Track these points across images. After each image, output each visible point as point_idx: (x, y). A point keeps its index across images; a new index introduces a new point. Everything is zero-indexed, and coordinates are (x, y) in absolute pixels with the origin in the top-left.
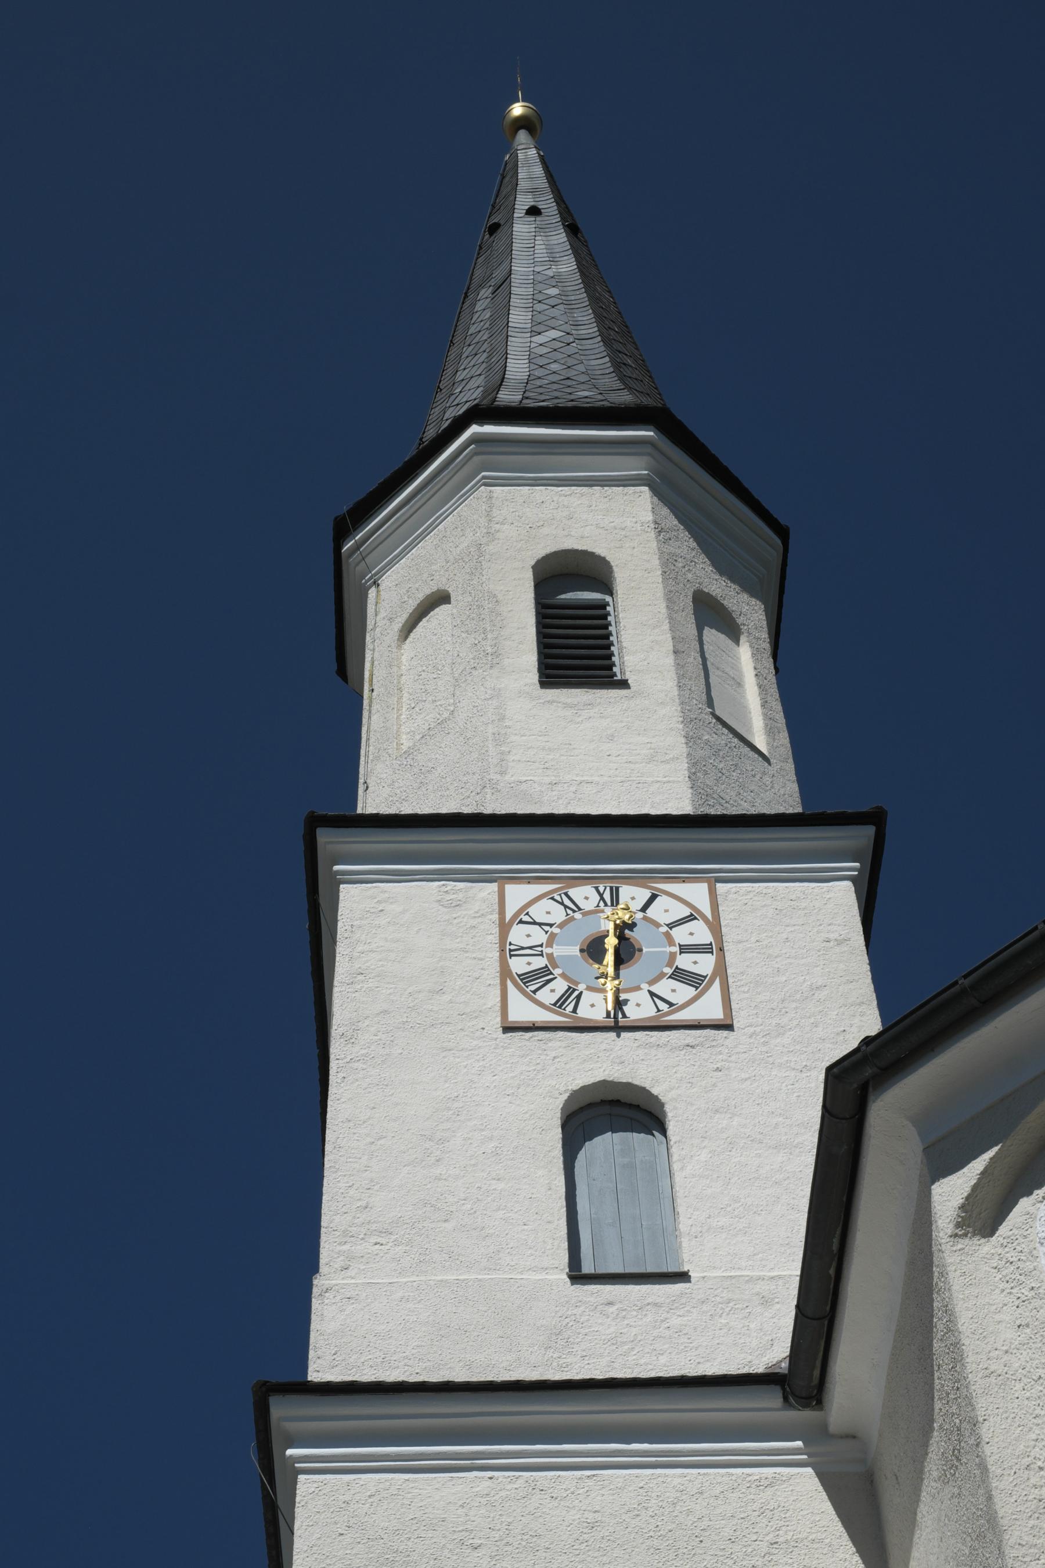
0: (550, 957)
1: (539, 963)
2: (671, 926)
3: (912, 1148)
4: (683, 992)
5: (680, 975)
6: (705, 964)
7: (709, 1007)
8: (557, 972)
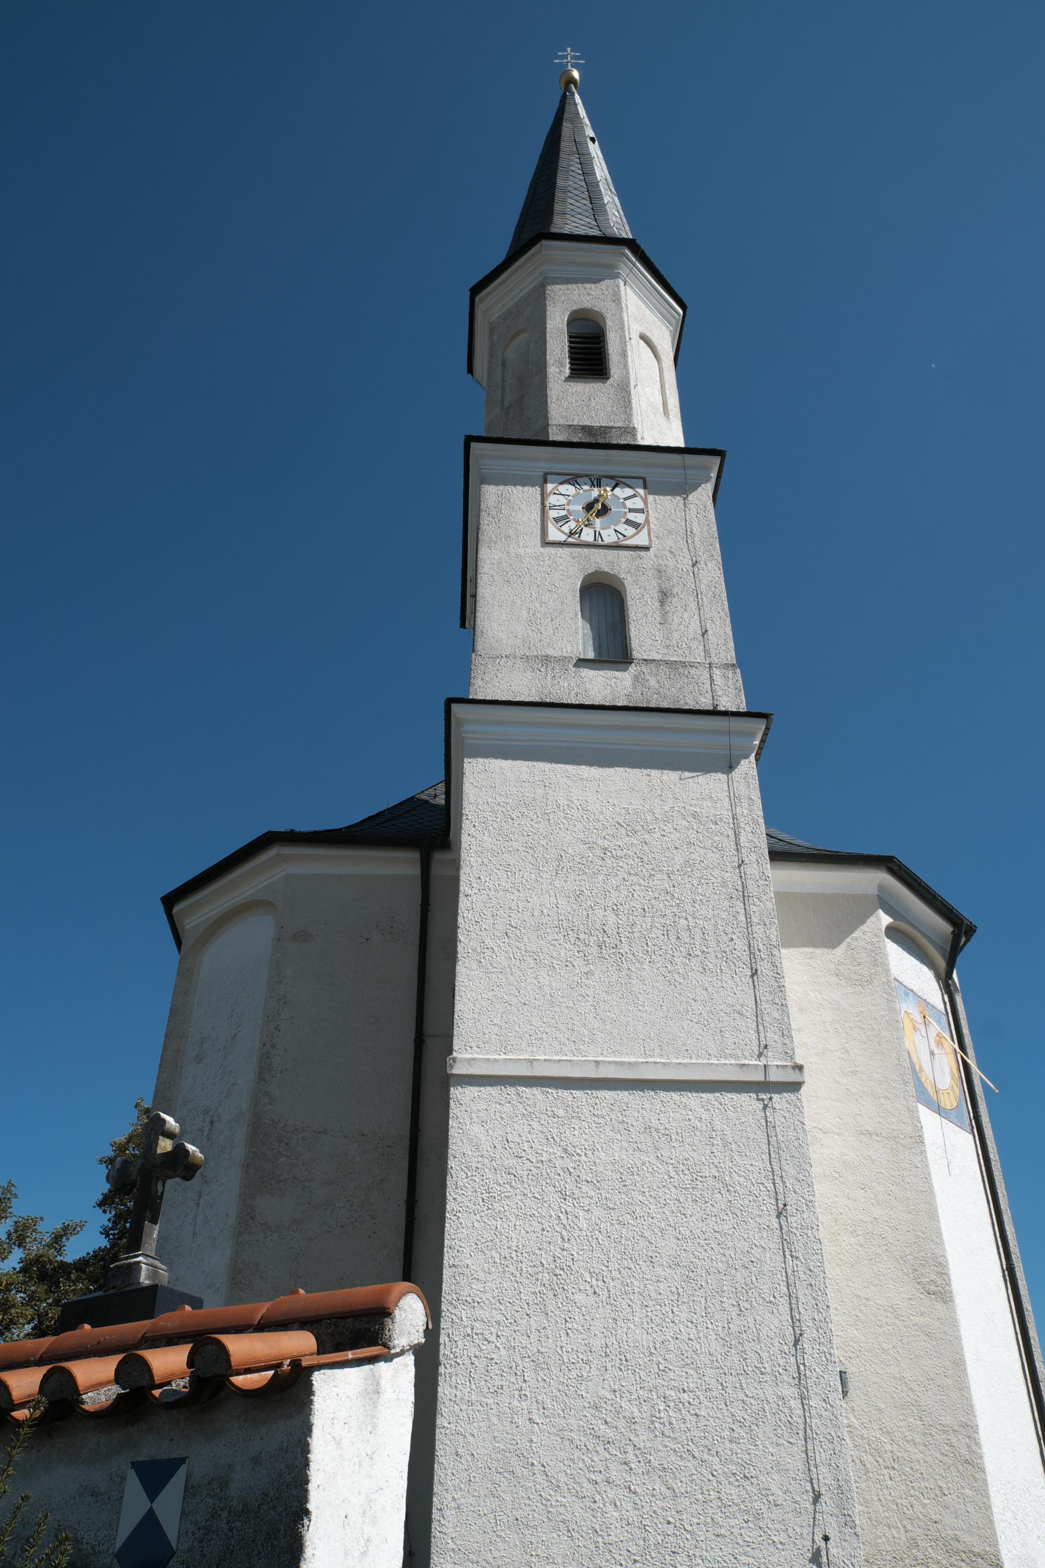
0: (568, 510)
1: (563, 513)
2: (626, 499)
3: (873, 891)
4: (630, 531)
5: (629, 522)
6: (640, 518)
7: (641, 539)
8: (571, 518)
